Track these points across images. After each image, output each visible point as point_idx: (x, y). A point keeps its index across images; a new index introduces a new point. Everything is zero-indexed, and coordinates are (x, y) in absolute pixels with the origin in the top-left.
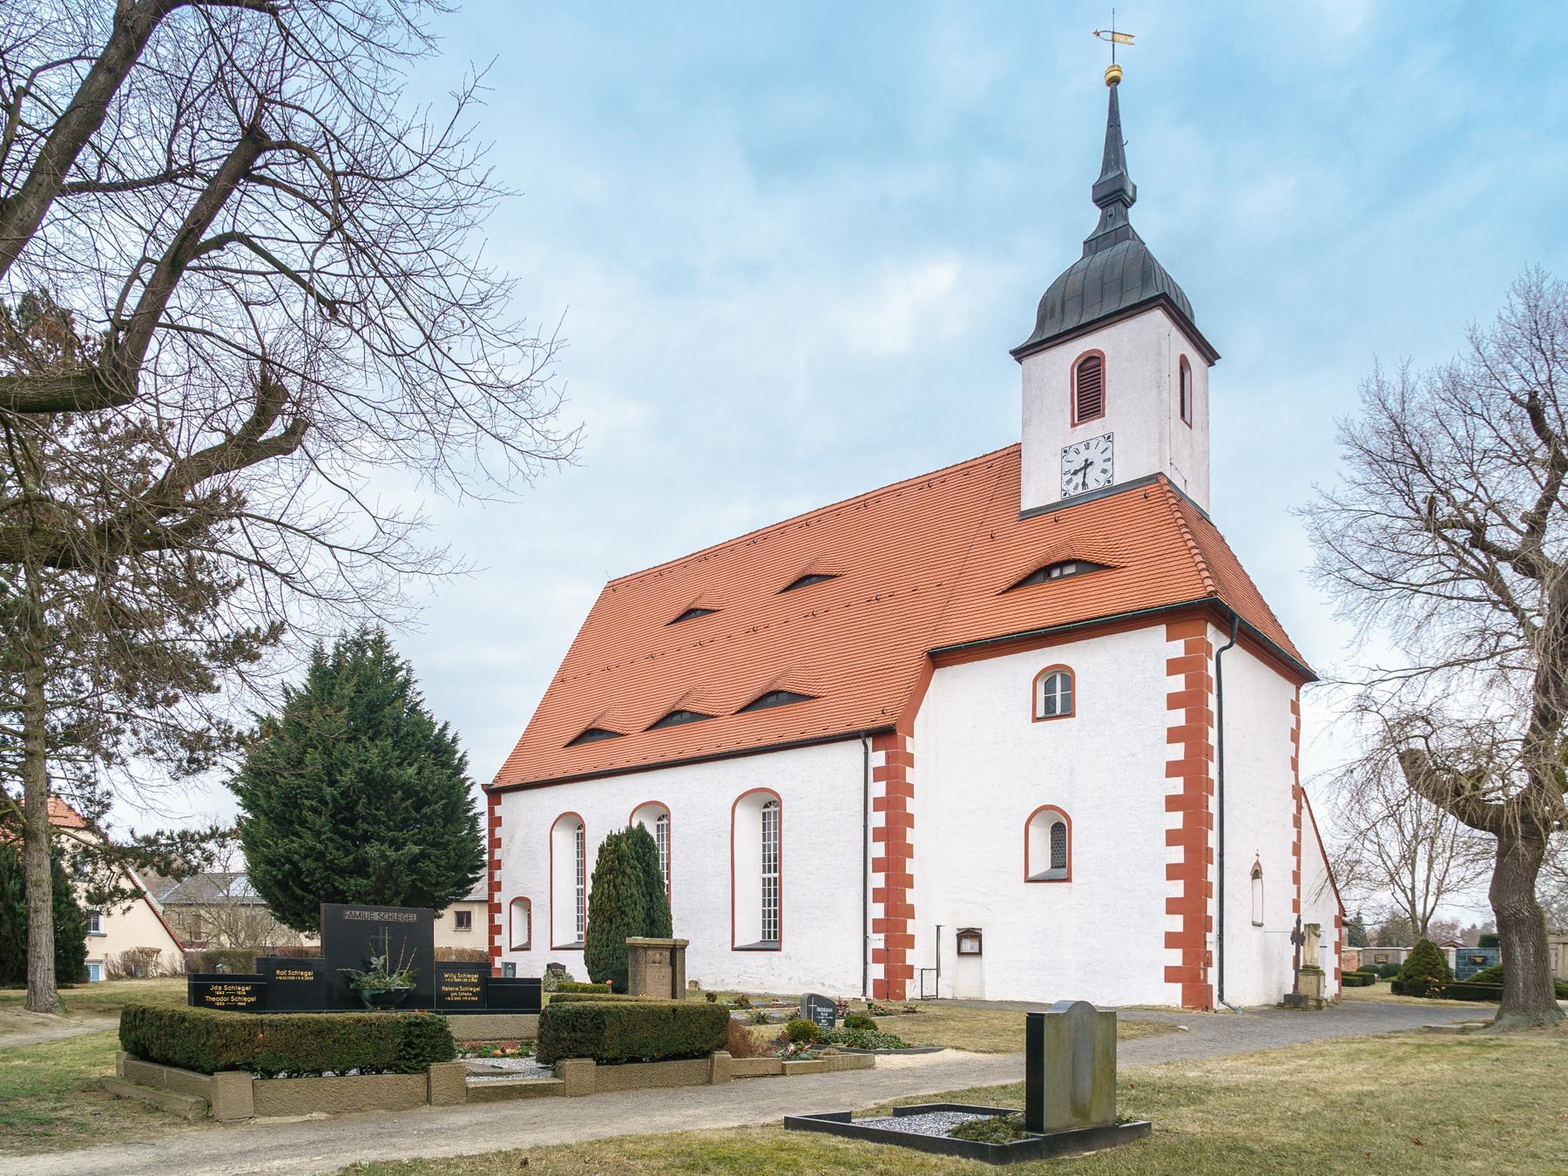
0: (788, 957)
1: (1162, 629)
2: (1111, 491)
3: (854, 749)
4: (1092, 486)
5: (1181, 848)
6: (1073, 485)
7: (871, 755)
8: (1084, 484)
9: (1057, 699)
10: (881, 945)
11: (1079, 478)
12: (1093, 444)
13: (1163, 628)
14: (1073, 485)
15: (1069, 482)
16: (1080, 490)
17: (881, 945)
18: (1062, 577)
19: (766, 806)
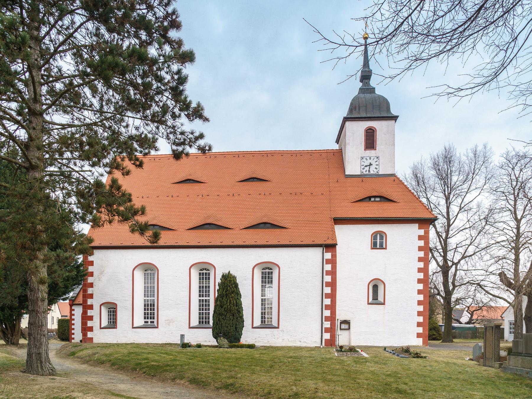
0: (283, 331)
1: (417, 225)
2: (378, 176)
3: (319, 251)
4: (372, 172)
5: (422, 295)
6: (365, 170)
7: (325, 254)
8: (369, 171)
9: (378, 243)
10: (329, 326)
11: (367, 168)
12: (372, 158)
13: (417, 225)
14: (365, 170)
15: (363, 169)
16: (367, 172)
17: (329, 326)
18: (375, 201)
19: (201, 270)
